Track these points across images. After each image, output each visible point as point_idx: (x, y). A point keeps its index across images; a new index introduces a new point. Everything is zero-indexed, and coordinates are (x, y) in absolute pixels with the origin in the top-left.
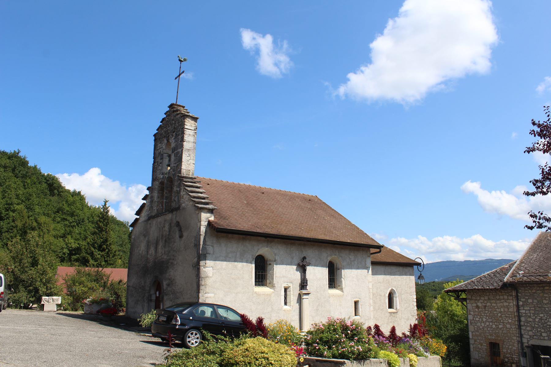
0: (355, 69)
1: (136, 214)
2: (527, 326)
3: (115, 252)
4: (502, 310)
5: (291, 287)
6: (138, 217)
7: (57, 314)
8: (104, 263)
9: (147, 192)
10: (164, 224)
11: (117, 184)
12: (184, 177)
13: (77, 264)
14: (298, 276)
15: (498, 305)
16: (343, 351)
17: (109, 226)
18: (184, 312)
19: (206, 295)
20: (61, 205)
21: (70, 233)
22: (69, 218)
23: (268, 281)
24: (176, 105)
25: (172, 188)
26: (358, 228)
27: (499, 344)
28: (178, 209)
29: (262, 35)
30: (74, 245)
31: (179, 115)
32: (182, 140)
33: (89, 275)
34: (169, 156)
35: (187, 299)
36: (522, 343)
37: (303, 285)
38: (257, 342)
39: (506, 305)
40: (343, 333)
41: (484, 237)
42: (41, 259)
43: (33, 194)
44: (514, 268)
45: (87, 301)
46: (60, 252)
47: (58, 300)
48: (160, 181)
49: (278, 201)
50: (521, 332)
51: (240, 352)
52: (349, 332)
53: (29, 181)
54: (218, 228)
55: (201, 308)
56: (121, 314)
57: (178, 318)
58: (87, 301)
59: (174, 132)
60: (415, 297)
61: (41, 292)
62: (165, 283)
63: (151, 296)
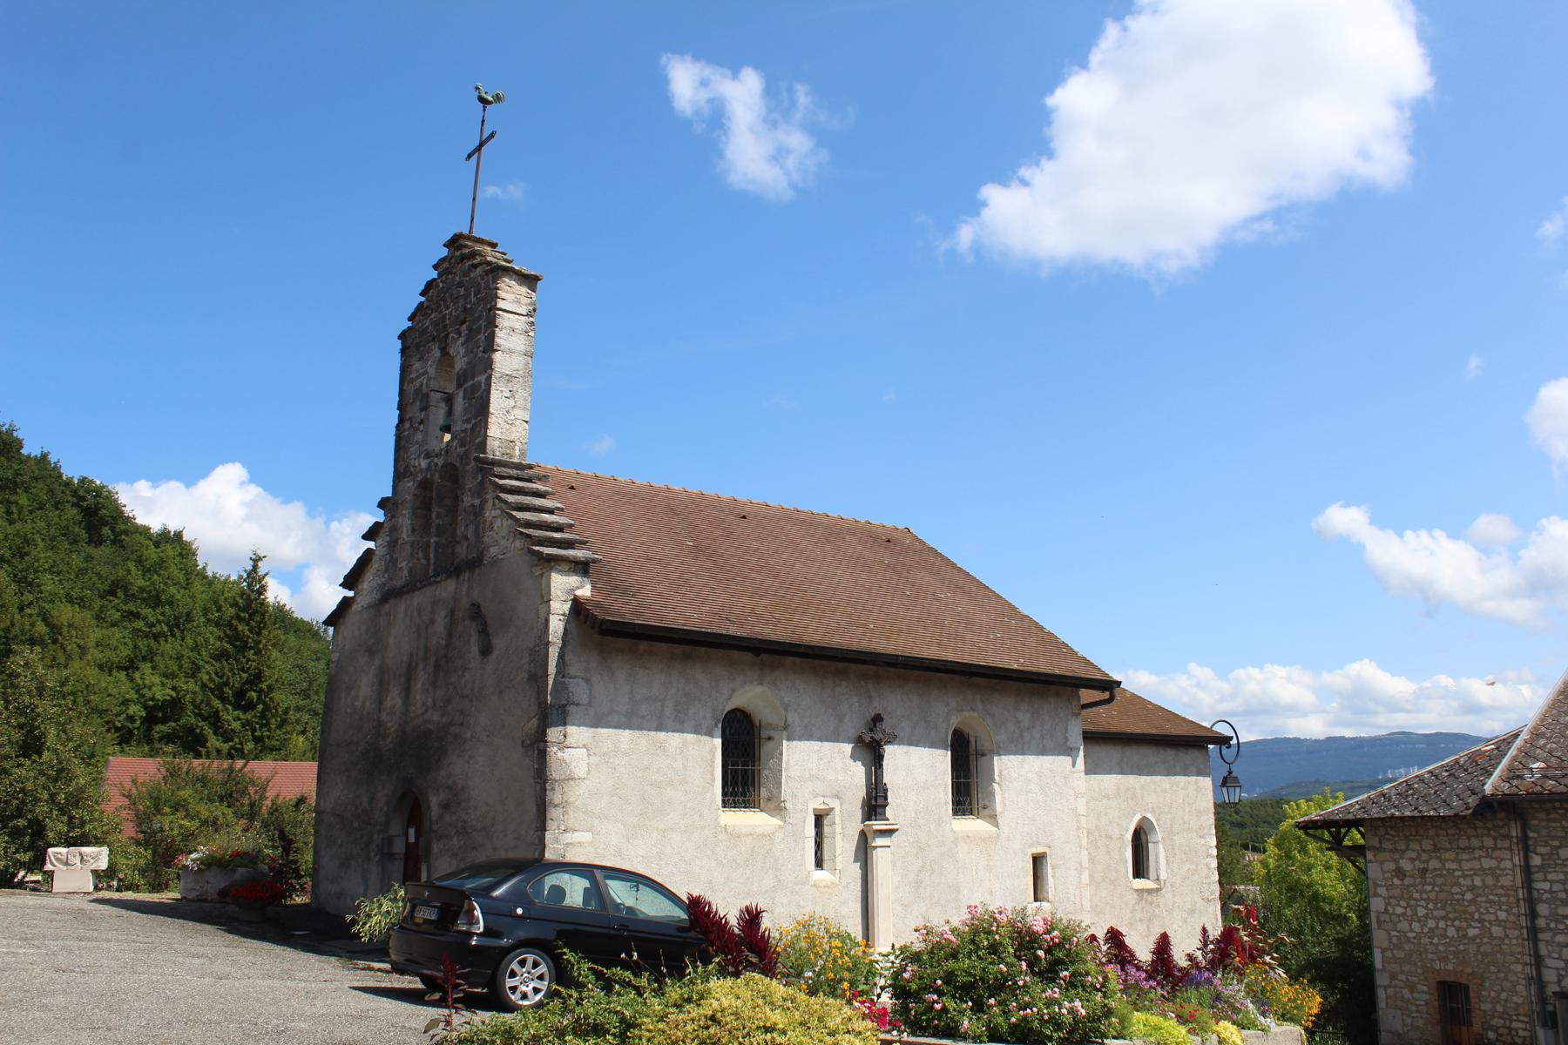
0: (1005, 175)
1: (344, 585)
2: (1555, 932)
3: (286, 712)
4: (1478, 881)
5: (837, 811)
6: (351, 594)
7: (94, 901)
8: (250, 746)
9: (380, 516)
10: (433, 613)
11: (296, 510)
12: (495, 463)
13: (169, 748)
14: (857, 773)
15: (1465, 866)
16: (1025, 1018)
17: (265, 632)
18: (497, 893)
19: (568, 837)
20: (121, 573)
21: (149, 657)
22: (145, 611)
23: (764, 793)
24: (469, 238)
25: (457, 498)
26: (1041, 628)
27: (1466, 987)
28: (475, 563)
29: (728, 73)
30: (161, 693)
31: (479, 270)
32: (490, 347)
33: (204, 780)
34: (449, 400)
35: (505, 847)
36: (1542, 986)
37: (875, 803)
38: (746, 994)
39: (1492, 866)
40: (1019, 959)
41: (1383, 666)
42: (52, 732)
43: (38, 538)
44: (1513, 751)
45: (189, 860)
46: (117, 715)
47: (100, 857)
48: (419, 478)
49: (792, 541)
50: (1536, 948)
51: (689, 1028)
52: (1041, 953)
53: (23, 500)
54: (604, 621)
55: (551, 880)
56: (298, 900)
57: (478, 912)
58: (189, 860)
59: (463, 323)
60: (1214, 842)
61: (51, 835)
62: (434, 801)
63: (389, 841)
